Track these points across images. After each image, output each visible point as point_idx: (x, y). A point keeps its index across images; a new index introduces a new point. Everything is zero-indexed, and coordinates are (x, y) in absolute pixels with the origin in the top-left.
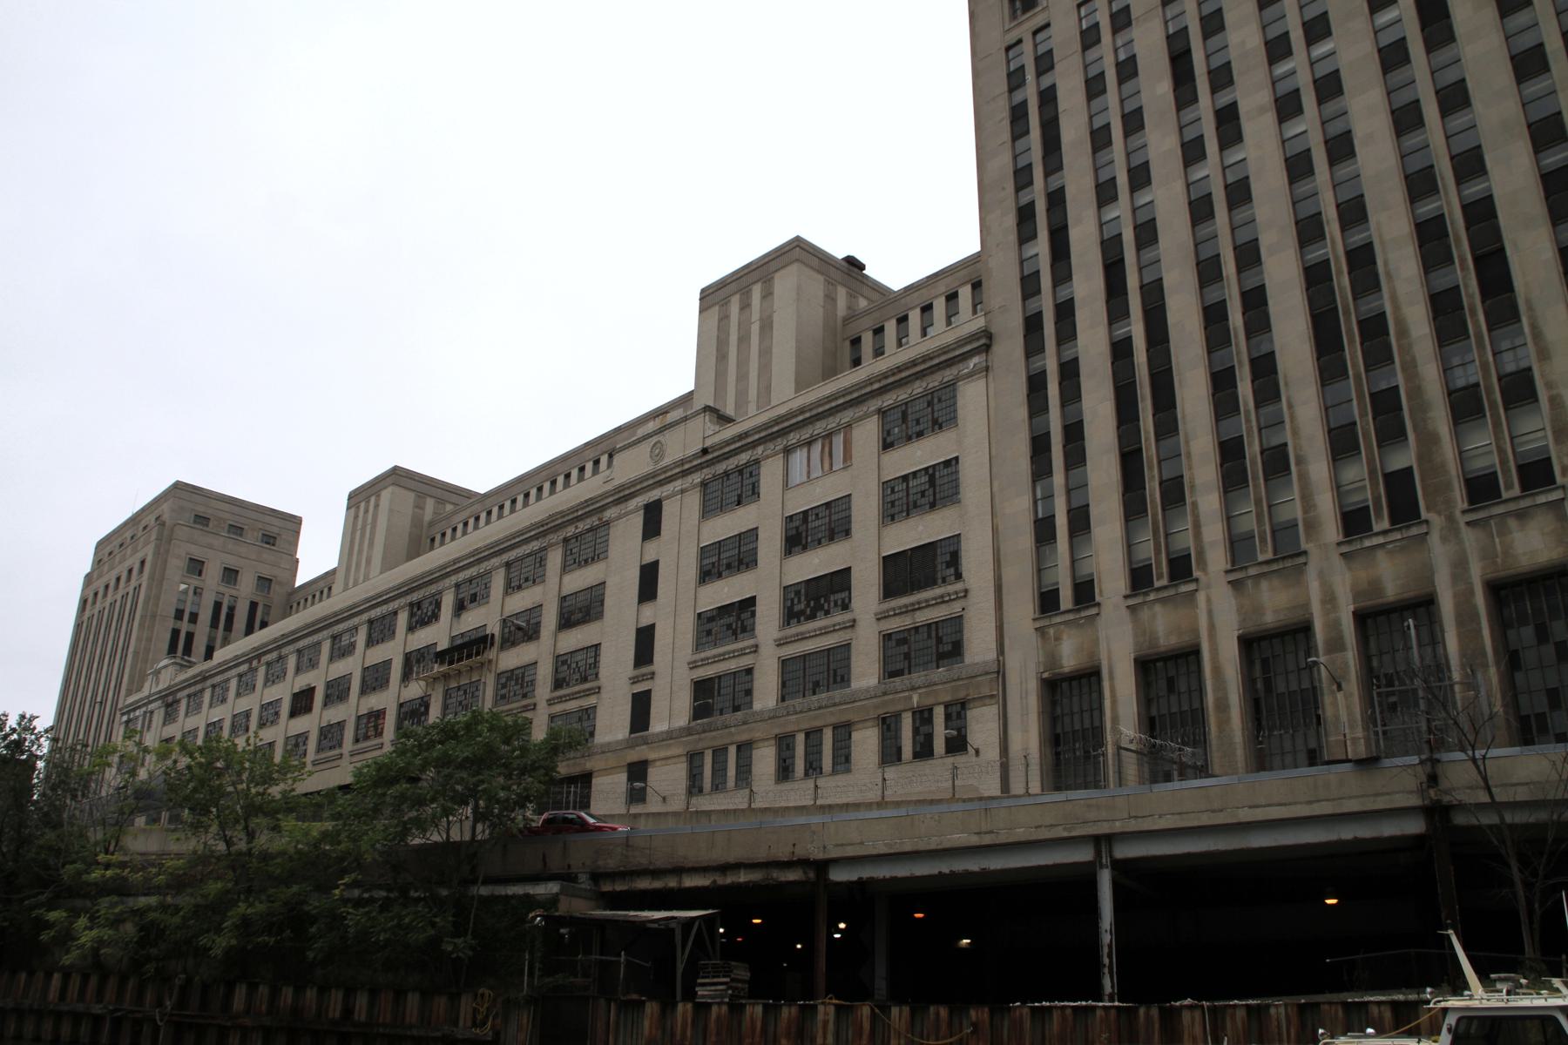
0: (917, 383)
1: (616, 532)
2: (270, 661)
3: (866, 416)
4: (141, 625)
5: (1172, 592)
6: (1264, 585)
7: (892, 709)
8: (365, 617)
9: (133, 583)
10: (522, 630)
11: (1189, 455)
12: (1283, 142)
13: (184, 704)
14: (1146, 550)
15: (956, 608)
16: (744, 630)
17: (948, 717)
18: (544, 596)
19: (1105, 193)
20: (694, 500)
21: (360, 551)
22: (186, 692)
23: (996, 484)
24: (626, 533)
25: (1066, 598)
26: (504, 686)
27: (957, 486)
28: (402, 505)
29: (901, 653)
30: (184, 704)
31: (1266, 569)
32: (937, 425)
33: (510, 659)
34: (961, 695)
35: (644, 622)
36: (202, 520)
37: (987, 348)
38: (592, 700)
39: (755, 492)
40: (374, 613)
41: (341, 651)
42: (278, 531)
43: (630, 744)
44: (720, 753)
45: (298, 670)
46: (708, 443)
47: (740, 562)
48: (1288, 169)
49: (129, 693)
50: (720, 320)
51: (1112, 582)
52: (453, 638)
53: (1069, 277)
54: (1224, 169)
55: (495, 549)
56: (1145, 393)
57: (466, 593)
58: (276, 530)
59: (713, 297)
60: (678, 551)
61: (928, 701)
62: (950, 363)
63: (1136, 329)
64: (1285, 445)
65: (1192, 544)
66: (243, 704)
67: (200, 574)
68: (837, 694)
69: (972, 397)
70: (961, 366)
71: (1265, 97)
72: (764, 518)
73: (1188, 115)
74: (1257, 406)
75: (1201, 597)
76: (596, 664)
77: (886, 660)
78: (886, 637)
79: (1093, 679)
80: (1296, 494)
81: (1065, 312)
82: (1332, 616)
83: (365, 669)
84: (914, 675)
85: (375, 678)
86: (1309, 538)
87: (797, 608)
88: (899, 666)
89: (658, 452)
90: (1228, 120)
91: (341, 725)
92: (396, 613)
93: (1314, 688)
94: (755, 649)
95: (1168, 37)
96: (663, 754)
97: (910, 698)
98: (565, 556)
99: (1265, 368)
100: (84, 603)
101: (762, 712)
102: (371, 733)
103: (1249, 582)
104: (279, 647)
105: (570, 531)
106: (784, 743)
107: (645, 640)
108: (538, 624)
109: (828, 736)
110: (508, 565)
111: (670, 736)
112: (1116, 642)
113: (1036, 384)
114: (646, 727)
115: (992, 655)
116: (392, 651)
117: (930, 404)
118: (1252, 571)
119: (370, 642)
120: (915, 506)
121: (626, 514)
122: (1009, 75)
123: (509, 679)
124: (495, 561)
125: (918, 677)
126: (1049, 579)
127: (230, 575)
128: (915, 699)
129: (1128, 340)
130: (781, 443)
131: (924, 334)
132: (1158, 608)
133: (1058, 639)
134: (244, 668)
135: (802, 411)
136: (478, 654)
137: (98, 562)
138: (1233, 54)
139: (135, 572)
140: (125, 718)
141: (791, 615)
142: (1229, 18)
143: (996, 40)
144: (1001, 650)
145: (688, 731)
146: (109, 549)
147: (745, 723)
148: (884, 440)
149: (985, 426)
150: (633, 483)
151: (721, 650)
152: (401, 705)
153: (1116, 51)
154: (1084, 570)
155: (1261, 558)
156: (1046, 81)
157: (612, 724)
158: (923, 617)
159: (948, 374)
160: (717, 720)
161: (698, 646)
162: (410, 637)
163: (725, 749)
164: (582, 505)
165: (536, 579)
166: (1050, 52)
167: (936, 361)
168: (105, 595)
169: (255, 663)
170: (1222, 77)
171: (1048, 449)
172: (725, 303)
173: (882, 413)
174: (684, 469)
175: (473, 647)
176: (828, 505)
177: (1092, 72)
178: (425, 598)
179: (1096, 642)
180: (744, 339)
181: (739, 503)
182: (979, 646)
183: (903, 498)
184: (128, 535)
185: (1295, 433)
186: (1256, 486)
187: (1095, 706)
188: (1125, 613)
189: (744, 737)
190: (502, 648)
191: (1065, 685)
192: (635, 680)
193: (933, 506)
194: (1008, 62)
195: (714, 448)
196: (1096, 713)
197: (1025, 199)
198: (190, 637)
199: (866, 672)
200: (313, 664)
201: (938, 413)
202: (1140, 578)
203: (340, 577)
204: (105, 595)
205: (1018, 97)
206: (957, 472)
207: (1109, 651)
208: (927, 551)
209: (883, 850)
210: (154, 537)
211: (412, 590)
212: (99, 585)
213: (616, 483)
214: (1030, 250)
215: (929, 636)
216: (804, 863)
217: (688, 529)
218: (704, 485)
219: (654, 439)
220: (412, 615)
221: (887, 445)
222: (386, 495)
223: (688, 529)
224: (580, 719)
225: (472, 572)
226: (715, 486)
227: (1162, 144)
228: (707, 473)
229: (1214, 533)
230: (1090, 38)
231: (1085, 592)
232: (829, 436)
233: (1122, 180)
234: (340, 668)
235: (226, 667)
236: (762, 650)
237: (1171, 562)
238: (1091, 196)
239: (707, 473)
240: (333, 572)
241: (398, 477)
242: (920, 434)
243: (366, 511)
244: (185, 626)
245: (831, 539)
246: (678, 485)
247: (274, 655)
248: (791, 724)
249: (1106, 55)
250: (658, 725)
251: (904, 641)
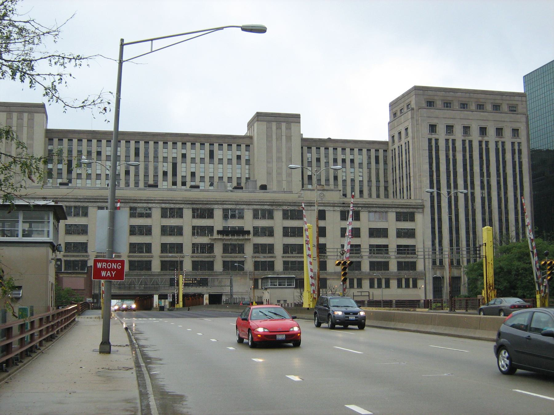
7: (400, 277)
61: (408, 277)
69: (418, 217)
159: (415, 210)
201: (411, 217)
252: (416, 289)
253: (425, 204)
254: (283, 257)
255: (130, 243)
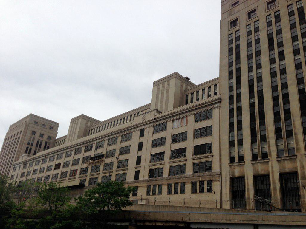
0: (203, 109)
1: (134, 134)
2: (51, 156)
3: (192, 114)
4: (19, 146)
5: (263, 161)
6: (286, 162)
7: (195, 180)
8: (75, 148)
9: (18, 136)
10: (111, 154)
11: (268, 130)
12: (295, 60)
13: (28, 164)
14: (256, 151)
15: (210, 159)
16: (161, 159)
17: (208, 184)
18: (116, 147)
19: (250, 69)
20: (151, 129)
21: (73, 132)
22: (29, 162)
23: (221, 132)
24: (136, 135)
25: (237, 160)
26: (106, 166)
27: (212, 132)
28: (85, 124)
29: (197, 168)
30: (28, 164)
31: (286, 158)
32: (208, 118)
33: (108, 161)
34: (211, 179)
35: (139, 155)
36: (36, 123)
37: (220, 102)
38: (126, 171)
39: (166, 129)
40: (76, 148)
41: (68, 156)
42: (53, 126)
43: (134, 182)
44: (154, 186)
45: (57, 159)
46: (155, 117)
47: (161, 144)
48: (296, 67)
49: (15, 161)
50: (158, 89)
51: (248, 157)
52: (95, 155)
53: (240, 88)
54: (280, 66)
55: (106, 136)
56: (258, 115)
57: (98, 145)
58: (53, 126)
59: (156, 84)
60: (147, 140)
61: (203, 180)
62: (212, 104)
63: (256, 100)
64: (292, 130)
65: (268, 150)
66: (43, 166)
67: (34, 135)
68: (182, 175)
69: (216, 113)
70: (214, 105)
71: (291, 50)
72: (167, 134)
73: (272, 53)
74: (285, 121)
75: (270, 163)
76: (127, 163)
77: (194, 169)
78: (194, 164)
79: (243, 179)
80: (294, 142)
81: (239, 96)
82: (303, 171)
83: (73, 160)
84: (200, 173)
85: (76, 162)
86: (297, 152)
87: (174, 155)
88: (197, 171)
89: (144, 118)
90: (282, 55)
91: (66, 172)
92: (82, 148)
93: (298, 187)
94: (164, 163)
95: (268, 34)
96: (141, 185)
97: (199, 178)
98: (122, 139)
99: (288, 112)
100: (6, 139)
101: (165, 178)
102: (74, 175)
103: (282, 161)
104: (53, 153)
105: (123, 133)
106: (169, 185)
107: (139, 159)
108: (115, 153)
109: (180, 185)
110: (109, 139)
111: (143, 181)
112: (249, 171)
113: (231, 111)
114: (138, 179)
115: (219, 171)
116: (80, 156)
117: (206, 113)
118: (283, 158)
119: (75, 154)
120: (202, 135)
121: (136, 131)
122: (229, 41)
123: (107, 165)
124: (106, 138)
125: (201, 174)
126: (233, 154)
127: (42, 135)
128: (200, 178)
129: (254, 103)
130: (172, 119)
131: (202, 99)
132: (259, 164)
133: (234, 169)
134: (44, 157)
135: (177, 112)
136: (100, 159)
137: (10, 130)
138: (284, 39)
139: (10, 138)
140: (13, 167)
141: (172, 157)
142: (283, 31)
143: (227, 33)
144: (221, 170)
145: (147, 181)
146: (13, 128)
147: (161, 180)
148: (195, 120)
149: (219, 119)
150: (138, 124)
151: (156, 163)
152: (81, 169)
153: (255, 37)
154: (241, 153)
155: (285, 155)
156: (238, 43)
157: (130, 177)
158: (203, 160)
159: (211, 107)
160: (154, 179)
161: (151, 162)
162: (85, 153)
163: (156, 185)
164: (123, 128)
165: (114, 143)
166: (239, 36)
167: (208, 104)
168: (11, 138)
169: (47, 156)
170: (281, 44)
171: (233, 125)
172: (159, 85)
173: (195, 114)
174: (150, 122)
175: (100, 157)
176: (182, 133)
177: (249, 41)
178: (89, 145)
179: (244, 170)
180: (163, 93)
181: (162, 131)
182: (216, 168)
183: (199, 133)
184: (18, 125)
185: (295, 127)
186: (284, 139)
187: (243, 185)
188: (251, 165)
189: (160, 183)
190: (106, 158)
191: (236, 179)
192: (136, 168)
193: (206, 136)
194: (229, 38)
195: (157, 118)
196: (243, 187)
197: (231, 69)
198: (31, 149)
199: (189, 171)
200: (61, 158)
201: (208, 115)
202: (255, 157)
203: (68, 138)
204: (11, 138)
205: (231, 46)
206: (212, 129)
207: (247, 173)
208: (204, 145)
209: (203, 221)
210: (24, 126)
211: (86, 143)
212: (10, 136)
213: (135, 124)
214: (231, 81)
215: (204, 165)
216: (185, 222)
217: (150, 136)
218: (154, 126)
219: (144, 115)
220: (86, 149)
221: (196, 121)
222: (80, 120)
223: (150, 136)
224: (123, 175)
225: (101, 140)
226: (157, 126)
227: (265, 59)
228: (155, 124)
229: (273, 149)
230: (249, 33)
231: (241, 159)
232: (183, 118)
233: (255, 67)
234: (67, 159)
235: (40, 157)
236: (165, 164)
237: (262, 154)
238: (247, 70)
239: (155, 124)
240: (66, 136)
241: (83, 117)
242: (204, 120)
243: (75, 124)
244: (30, 146)
245: (182, 141)
246: (148, 126)
247: (52, 155)
248: (171, 181)
249: (253, 37)
250: (141, 178)
251: (198, 165)
252: (211, 194)
253: (153, 125)
254: (170, 163)
255: (194, 146)
